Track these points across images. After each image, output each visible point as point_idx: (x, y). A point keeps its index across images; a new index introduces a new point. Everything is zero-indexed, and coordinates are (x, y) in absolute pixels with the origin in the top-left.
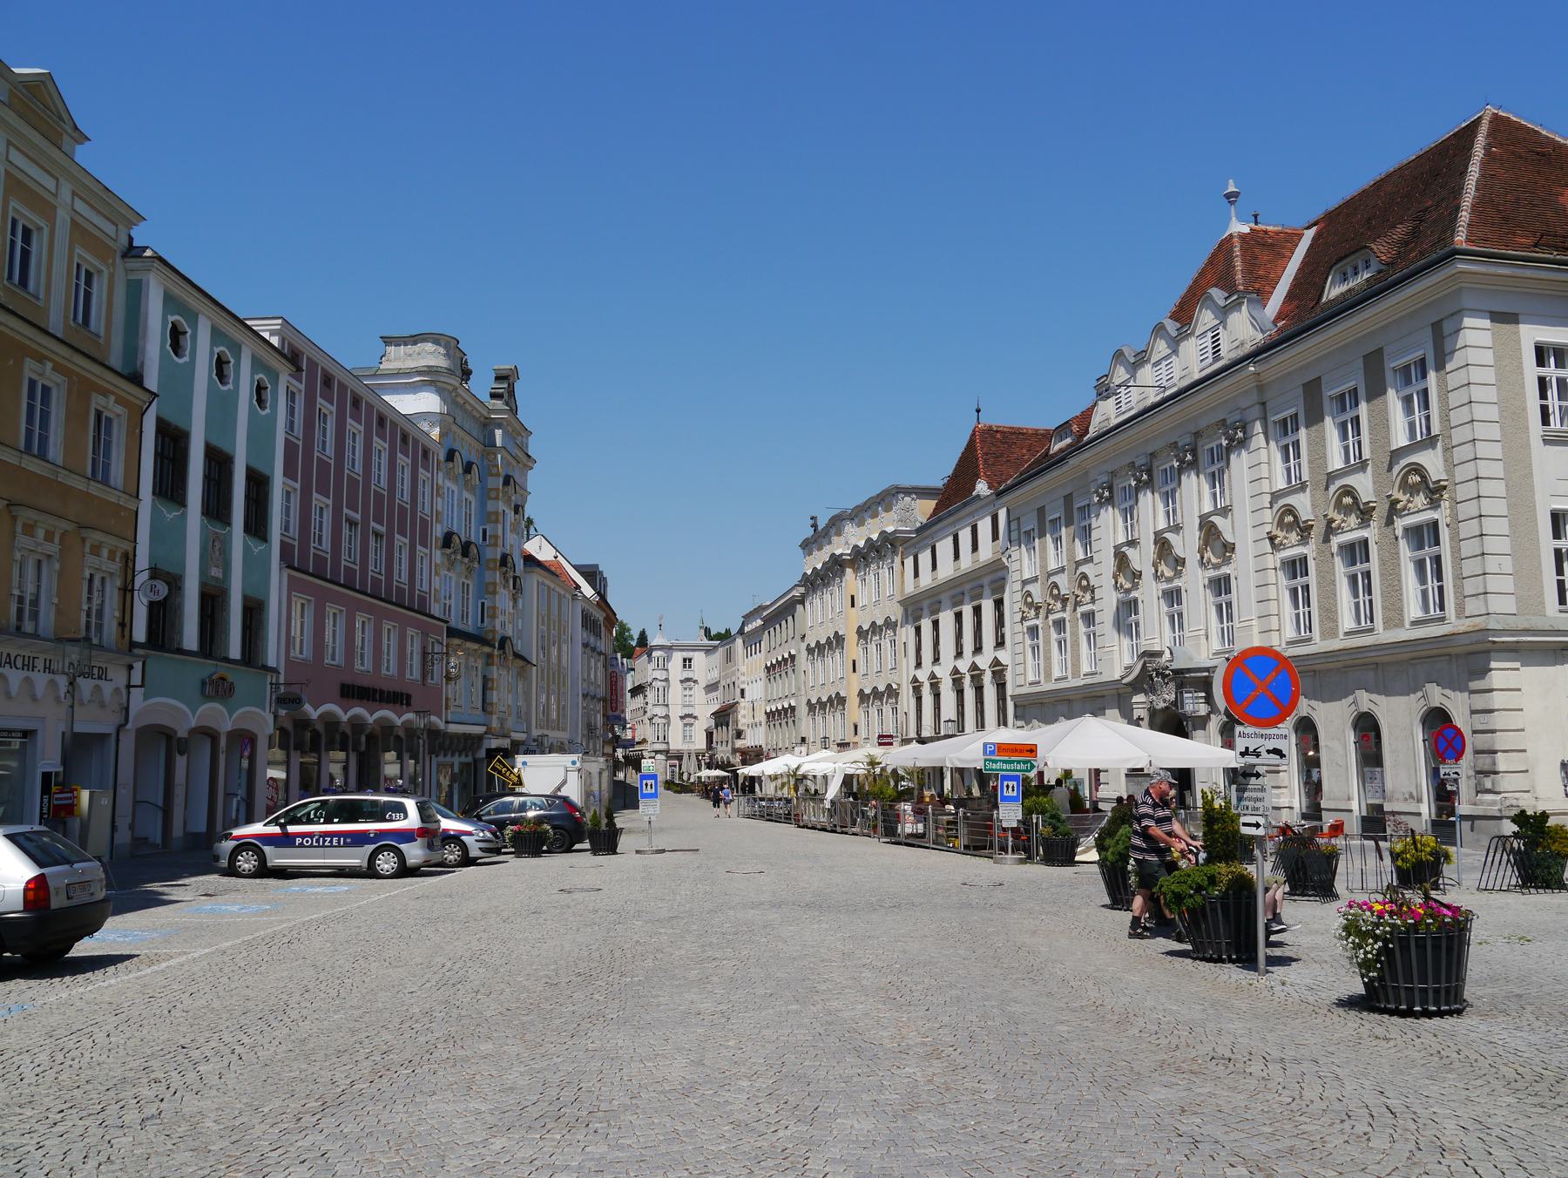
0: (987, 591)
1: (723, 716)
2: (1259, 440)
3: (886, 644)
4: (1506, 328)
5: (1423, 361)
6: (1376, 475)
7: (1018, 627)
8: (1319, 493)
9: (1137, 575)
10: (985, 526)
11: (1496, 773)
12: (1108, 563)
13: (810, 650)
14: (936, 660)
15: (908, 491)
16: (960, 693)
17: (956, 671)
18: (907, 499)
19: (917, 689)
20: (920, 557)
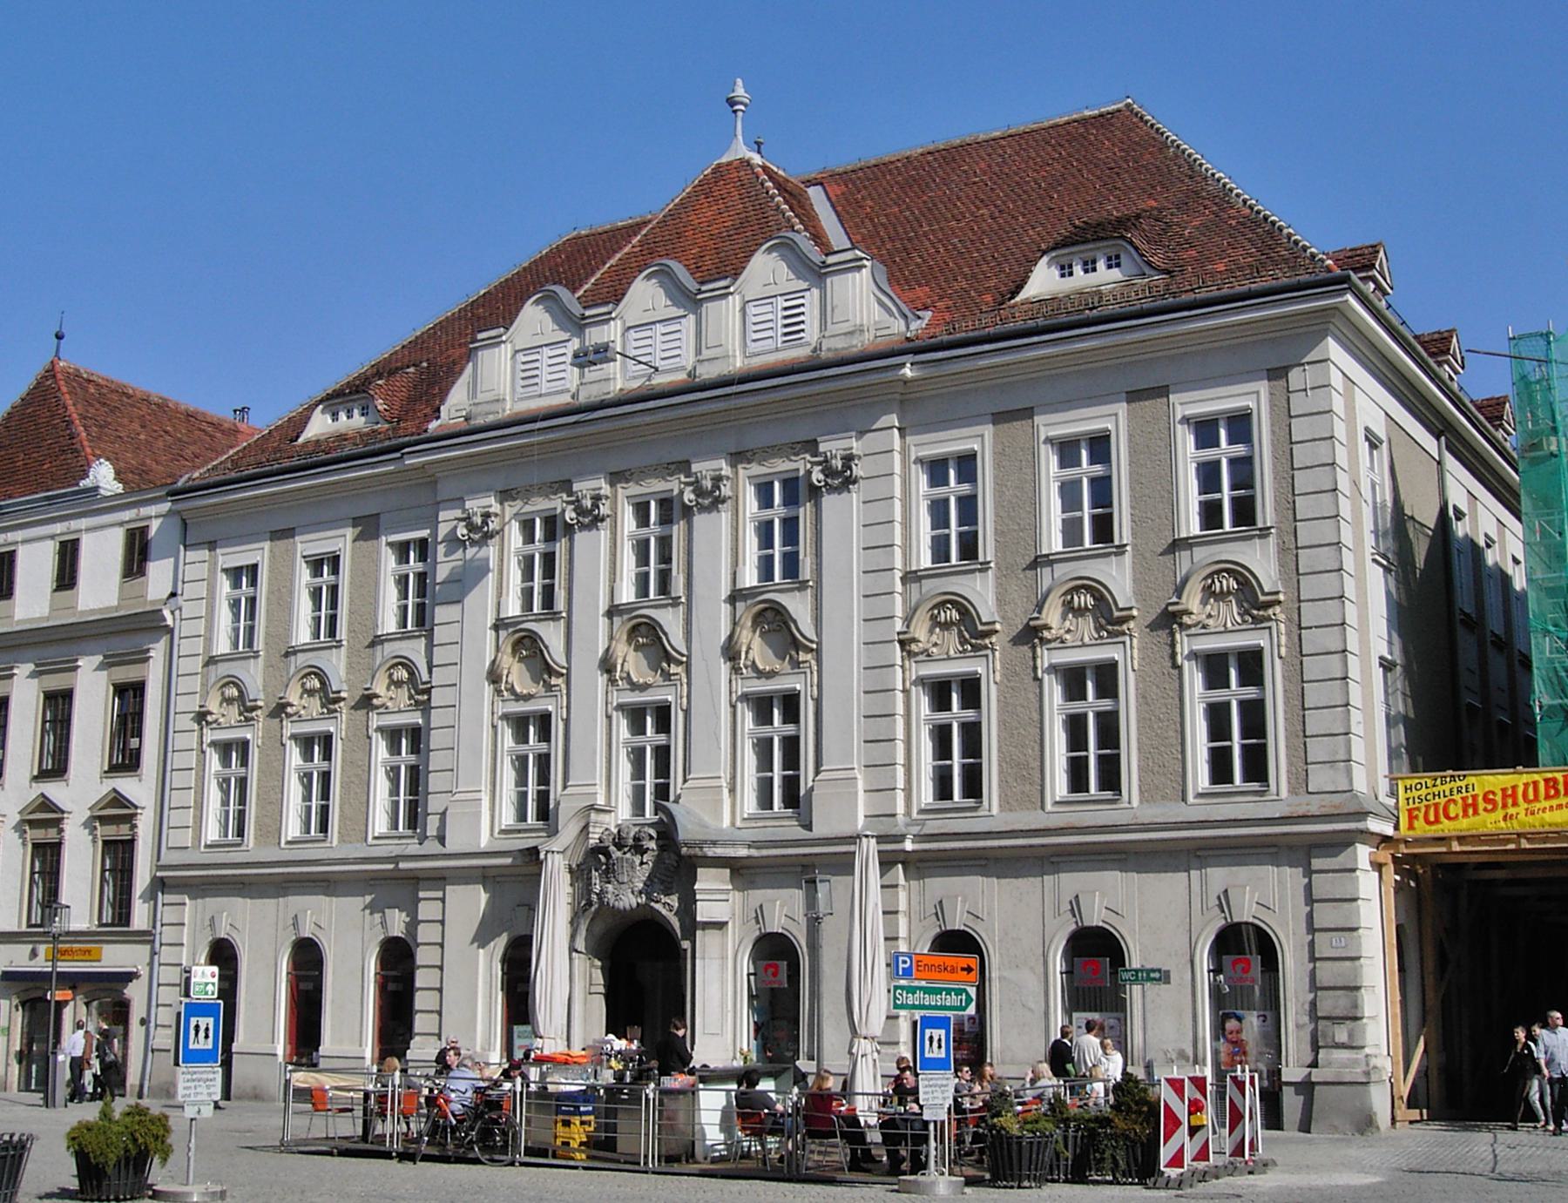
4: (282, 544)
6: (269, 666)
11: (1356, 1019)
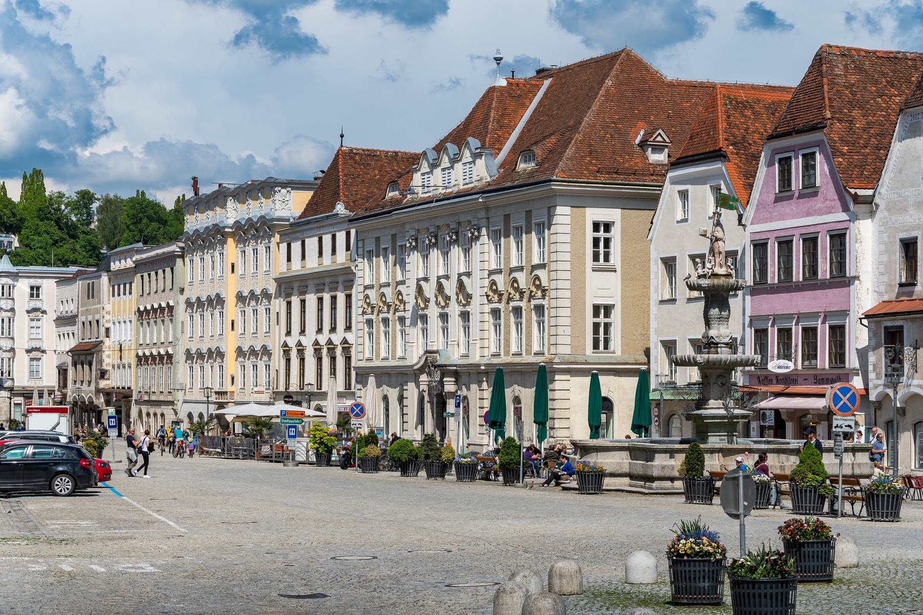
0: (341, 287)
1: (85, 355)
2: (484, 239)
3: (261, 309)
5: (544, 224)
7: (361, 318)
8: (507, 276)
9: (427, 301)
10: (341, 237)
12: (413, 290)
13: (189, 304)
14: (303, 332)
15: (285, 185)
16: (319, 359)
17: (316, 343)
18: (284, 191)
19: (287, 352)
20: (293, 245)
